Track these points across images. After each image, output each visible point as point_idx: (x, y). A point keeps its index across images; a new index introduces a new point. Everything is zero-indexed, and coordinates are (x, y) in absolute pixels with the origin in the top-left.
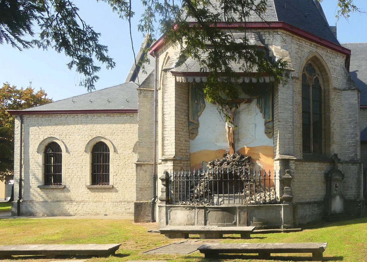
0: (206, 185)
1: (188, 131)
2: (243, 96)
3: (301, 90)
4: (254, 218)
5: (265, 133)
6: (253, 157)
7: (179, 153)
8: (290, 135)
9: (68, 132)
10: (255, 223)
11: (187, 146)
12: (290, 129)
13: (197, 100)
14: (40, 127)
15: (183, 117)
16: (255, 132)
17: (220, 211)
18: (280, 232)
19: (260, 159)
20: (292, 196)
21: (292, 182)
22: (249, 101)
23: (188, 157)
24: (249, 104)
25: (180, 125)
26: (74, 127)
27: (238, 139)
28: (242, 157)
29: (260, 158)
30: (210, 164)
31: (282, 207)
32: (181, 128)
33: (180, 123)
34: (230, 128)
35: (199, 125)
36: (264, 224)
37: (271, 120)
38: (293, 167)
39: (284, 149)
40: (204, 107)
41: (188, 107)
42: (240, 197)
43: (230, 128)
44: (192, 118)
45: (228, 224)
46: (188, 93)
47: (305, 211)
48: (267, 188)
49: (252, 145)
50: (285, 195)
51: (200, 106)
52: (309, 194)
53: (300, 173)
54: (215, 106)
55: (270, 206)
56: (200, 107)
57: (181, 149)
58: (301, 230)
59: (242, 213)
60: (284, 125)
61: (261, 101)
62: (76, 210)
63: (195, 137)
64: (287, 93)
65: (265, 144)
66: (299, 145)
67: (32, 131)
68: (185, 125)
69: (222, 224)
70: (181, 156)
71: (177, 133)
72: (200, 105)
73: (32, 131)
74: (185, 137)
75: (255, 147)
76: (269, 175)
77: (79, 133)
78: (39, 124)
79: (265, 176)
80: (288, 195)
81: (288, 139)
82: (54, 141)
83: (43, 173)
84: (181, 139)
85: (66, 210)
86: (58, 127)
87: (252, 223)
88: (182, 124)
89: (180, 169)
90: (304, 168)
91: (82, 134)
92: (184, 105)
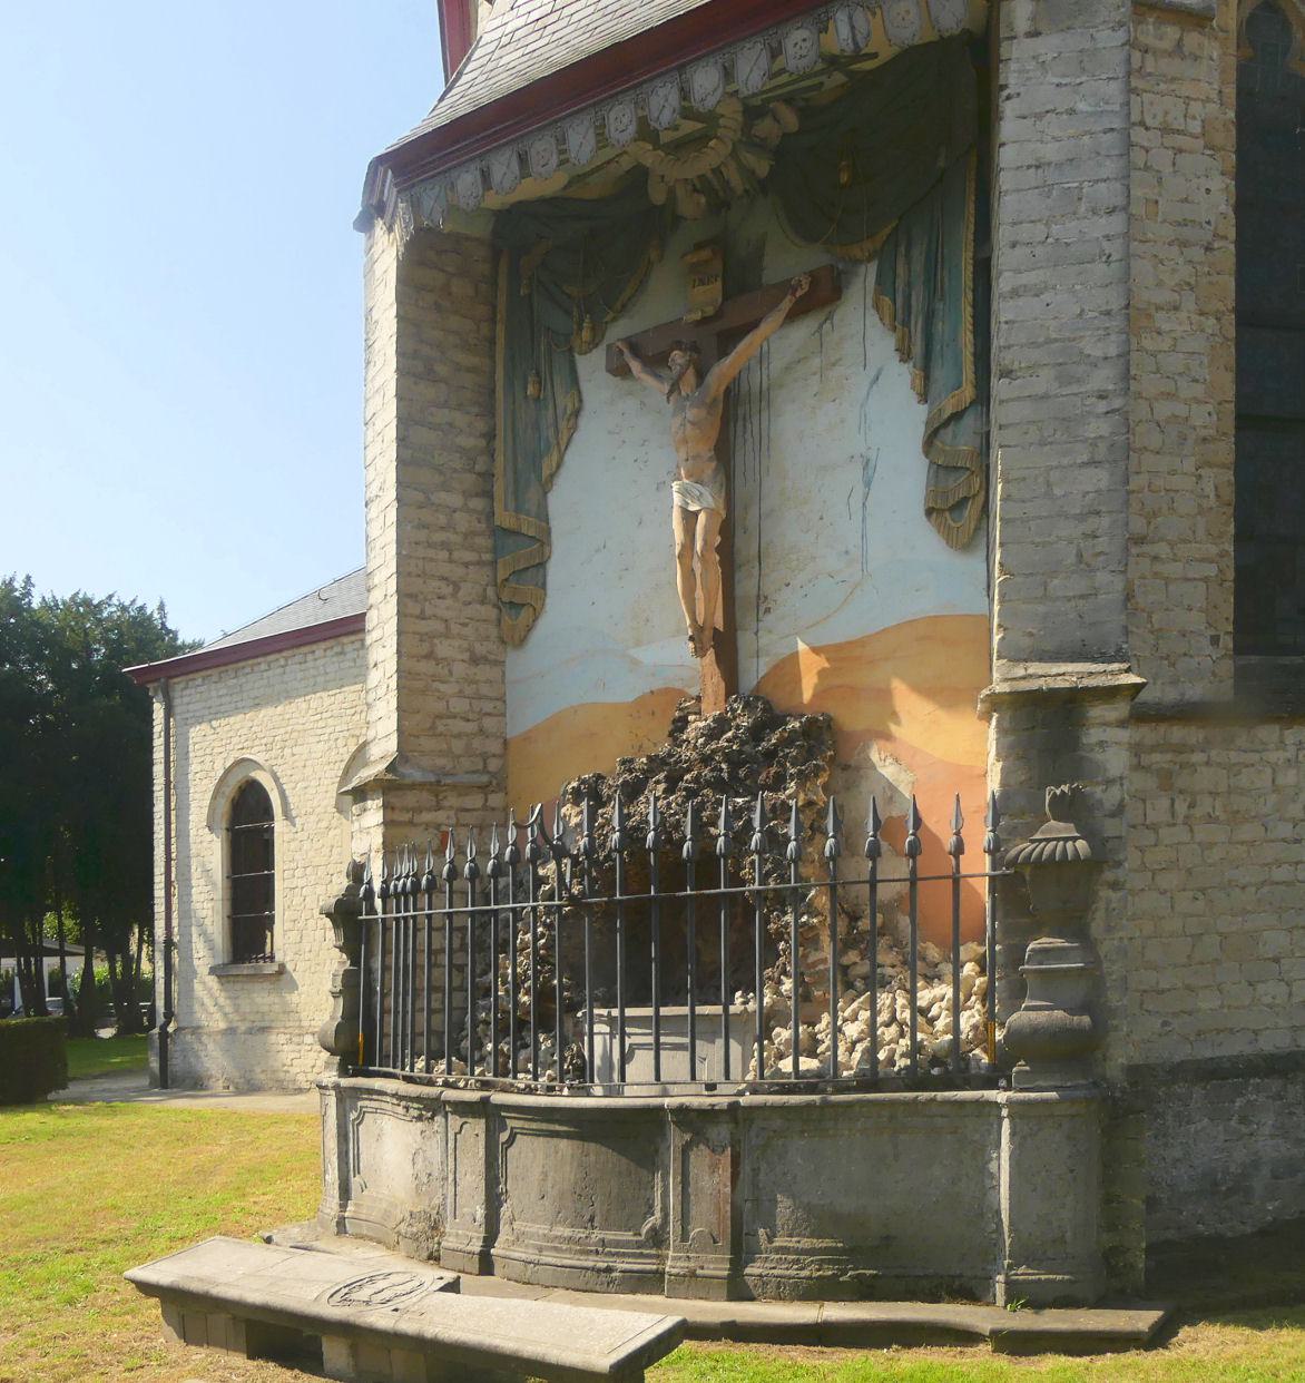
0: (543, 941)
1: (490, 592)
2: (789, 261)
3: (1232, 115)
4: (784, 1206)
5: (929, 512)
6: (851, 718)
7: (428, 744)
8: (1100, 478)
9: (289, 728)
10: (792, 1243)
11: (485, 690)
12: (1098, 428)
13: (538, 374)
14: (214, 723)
15: (455, 500)
16: (864, 520)
17: (567, 1136)
18: (963, 1337)
19: (893, 728)
20: (1086, 1019)
21: (1105, 893)
22: (820, 296)
23: (493, 765)
24: (821, 316)
25: (431, 553)
26: (304, 706)
27: (760, 598)
28: (770, 719)
29: (894, 716)
30: (577, 796)
31: (1001, 1119)
32: (443, 578)
33: (430, 545)
34: (696, 514)
35: (550, 545)
36: (853, 1254)
37: (968, 392)
38: (1116, 761)
39: (1041, 609)
40: (577, 413)
41: (490, 436)
42: (727, 1027)
43: (696, 514)
44: (511, 505)
45: (610, 1235)
46: (492, 341)
47: (1244, 1129)
48: (933, 952)
49: (843, 629)
50: (1026, 1016)
51: (551, 411)
52: (1283, 988)
53: (1210, 819)
54: (630, 393)
55: (905, 1103)
56: (551, 421)
57: (439, 717)
58: (1157, 1338)
59: (700, 1159)
60: (1045, 397)
61: (901, 270)
62: (313, 1067)
63: (529, 629)
64: (1072, 112)
65: (925, 605)
66: (1202, 586)
67: (195, 744)
68: (469, 556)
69: (581, 1233)
70: (441, 762)
71: (414, 609)
72: (551, 406)
73: (195, 744)
74: (467, 631)
75: (861, 643)
76: (949, 842)
77: (319, 732)
78: (211, 710)
79: (914, 851)
80: (1058, 1014)
81: (1081, 518)
82: (253, 774)
83: (227, 911)
84: (444, 649)
85: (286, 1068)
86: (263, 712)
87: (770, 1241)
88: (445, 545)
89: (436, 843)
90: (1244, 780)
91: (329, 730)
92: (460, 419)
